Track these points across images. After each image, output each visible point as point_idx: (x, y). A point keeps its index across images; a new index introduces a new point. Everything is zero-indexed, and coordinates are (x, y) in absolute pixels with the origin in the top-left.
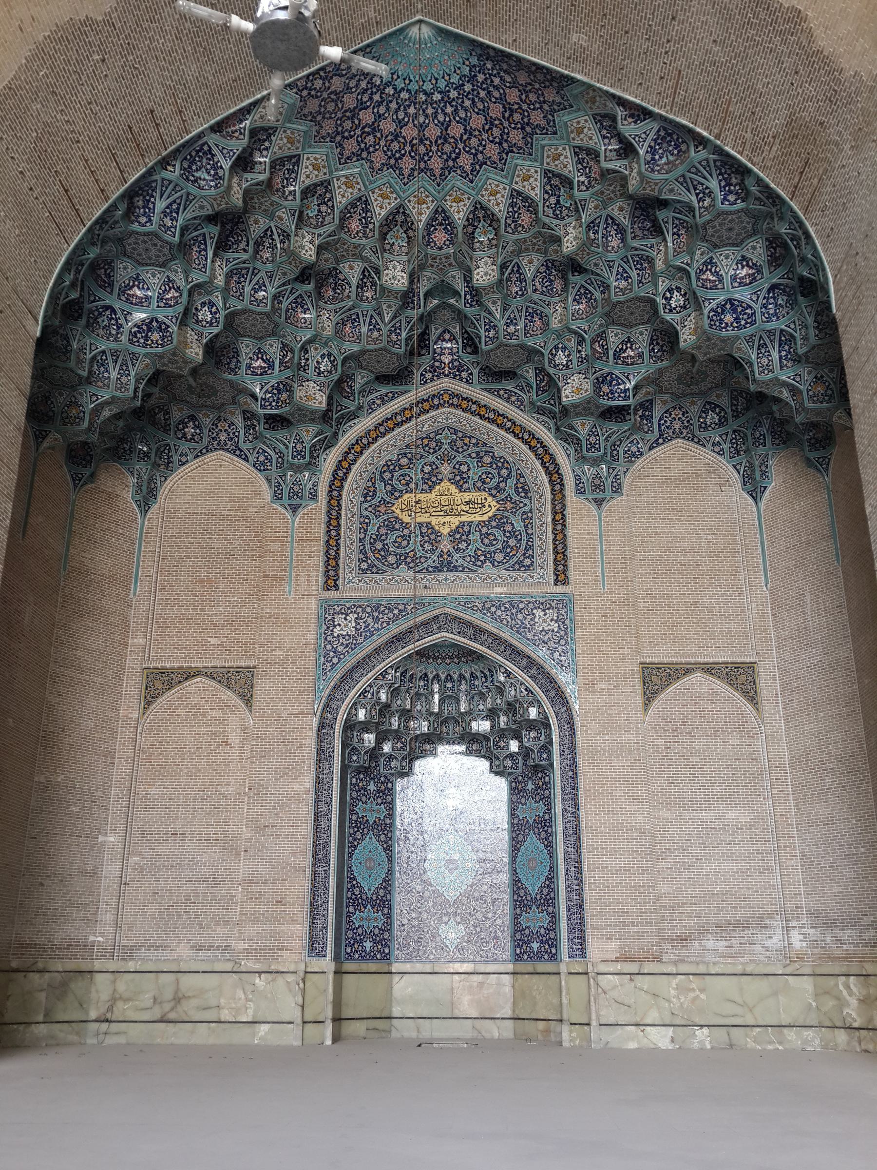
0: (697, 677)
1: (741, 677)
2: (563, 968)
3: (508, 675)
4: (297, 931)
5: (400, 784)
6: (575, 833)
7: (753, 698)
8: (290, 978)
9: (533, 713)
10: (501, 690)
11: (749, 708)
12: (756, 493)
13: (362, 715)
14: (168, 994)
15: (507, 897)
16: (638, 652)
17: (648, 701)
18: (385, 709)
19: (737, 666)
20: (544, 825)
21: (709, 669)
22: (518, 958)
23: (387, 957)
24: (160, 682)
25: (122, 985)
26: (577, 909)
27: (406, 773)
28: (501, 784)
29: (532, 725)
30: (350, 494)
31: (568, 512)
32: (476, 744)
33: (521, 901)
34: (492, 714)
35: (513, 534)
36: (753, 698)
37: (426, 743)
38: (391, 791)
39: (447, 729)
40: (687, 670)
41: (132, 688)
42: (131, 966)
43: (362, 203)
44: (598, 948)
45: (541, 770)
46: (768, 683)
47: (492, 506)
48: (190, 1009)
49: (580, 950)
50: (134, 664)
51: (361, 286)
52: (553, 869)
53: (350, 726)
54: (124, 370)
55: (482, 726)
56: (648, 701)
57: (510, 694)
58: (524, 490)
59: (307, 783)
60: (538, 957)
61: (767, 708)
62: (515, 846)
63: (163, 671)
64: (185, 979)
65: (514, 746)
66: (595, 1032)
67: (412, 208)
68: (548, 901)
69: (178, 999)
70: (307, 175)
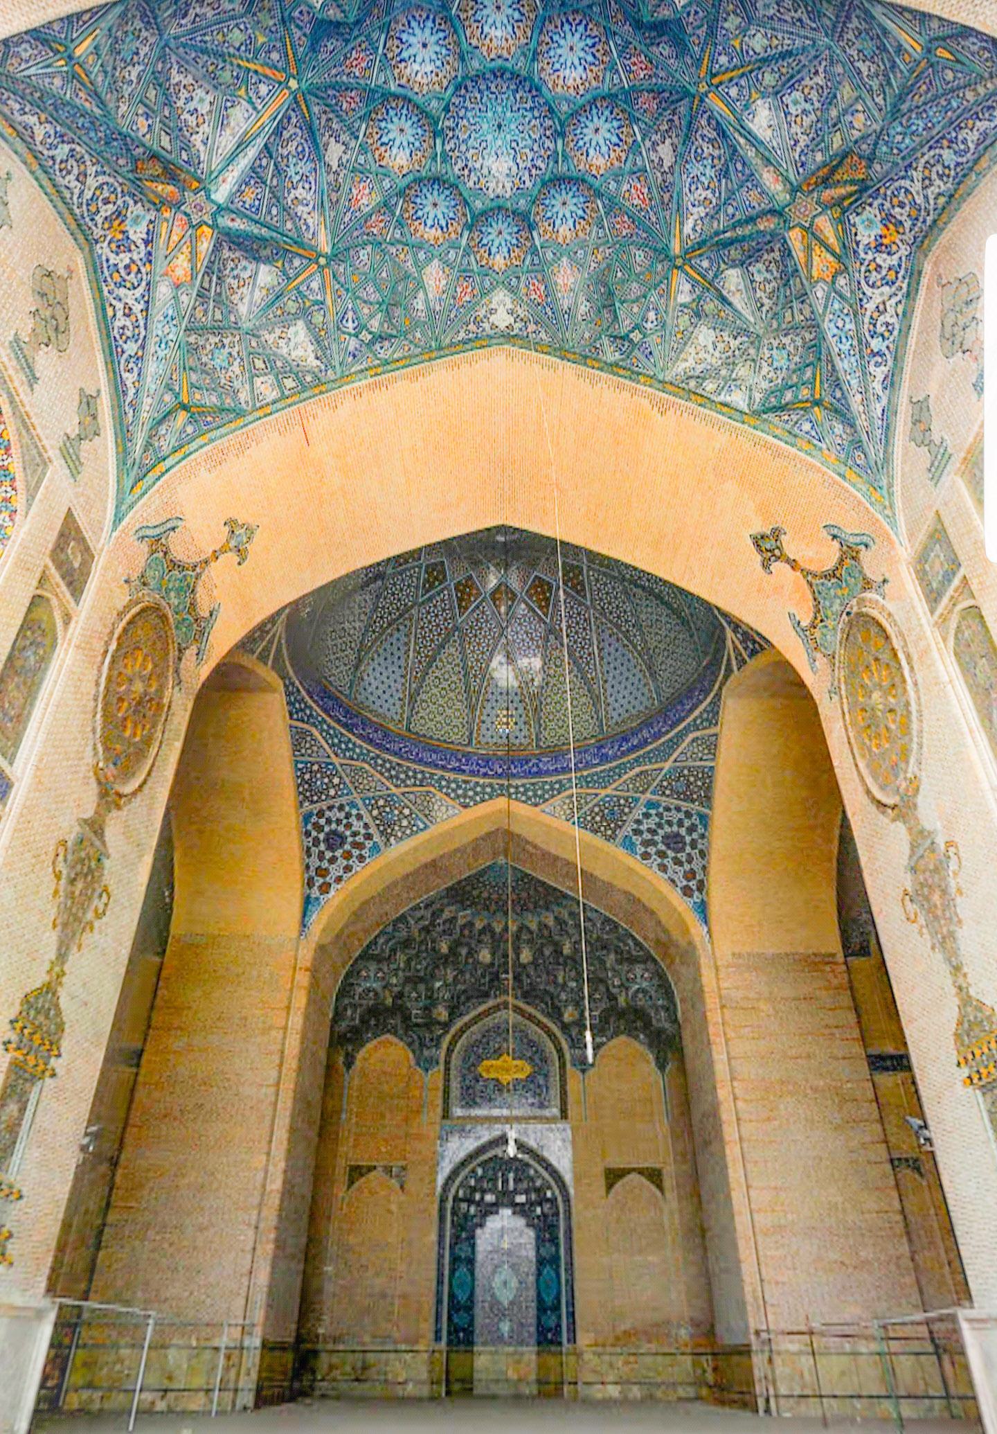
0: (634, 1177)
1: (655, 1176)
2: (564, 1350)
3: (536, 1171)
4: (427, 1327)
5: (478, 1231)
6: (570, 1264)
7: (660, 1187)
8: (453, 1356)
9: (549, 1194)
10: (532, 1179)
11: (658, 1193)
12: (662, 1066)
13: (461, 1194)
14: (359, 1364)
15: (534, 1305)
16: (603, 1160)
17: (608, 1192)
18: (474, 1190)
19: (654, 1170)
20: (555, 1260)
21: (641, 1172)
22: (539, 1343)
23: (471, 1343)
24: (356, 1172)
25: (335, 1359)
26: (572, 1315)
27: (481, 1225)
28: (531, 1233)
29: (548, 1200)
30: (455, 1060)
31: (568, 1076)
32: (519, 1210)
33: (542, 1308)
34: (527, 1192)
35: (539, 1086)
36: (660, 1187)
37: (492, 1209)
38: (473, 1237)
39: (506, 1200)
40: (630, 1171)
41: (341, 1175)
42: (341, 1347)
43: (471, 924)
44: (584, 1339)
45: (553, 1228)
46: (668, 1182)
47: (528, 1069)
48: (372, 1373)
49: (573, 1339)
50: (342, 1163)
51: (467, 958)
52: (559, 1293)
53: (456, 1199)
54: (354, 1012)
55: (521, 1199)
56: (608, 1192)
57: (538, 1183)
58: (545, 1060)
59: (434, 1237)
60: (551, 1342)
61: (668, 1194)
62: (539, 1274)
63: (358, 1167)
64: (369, 1355)
65: (539, 1210)
66: (580, 1387)
67: (495, 925)
68: (556, 1308)
69: (365, 1368)
70: (446, 915)
